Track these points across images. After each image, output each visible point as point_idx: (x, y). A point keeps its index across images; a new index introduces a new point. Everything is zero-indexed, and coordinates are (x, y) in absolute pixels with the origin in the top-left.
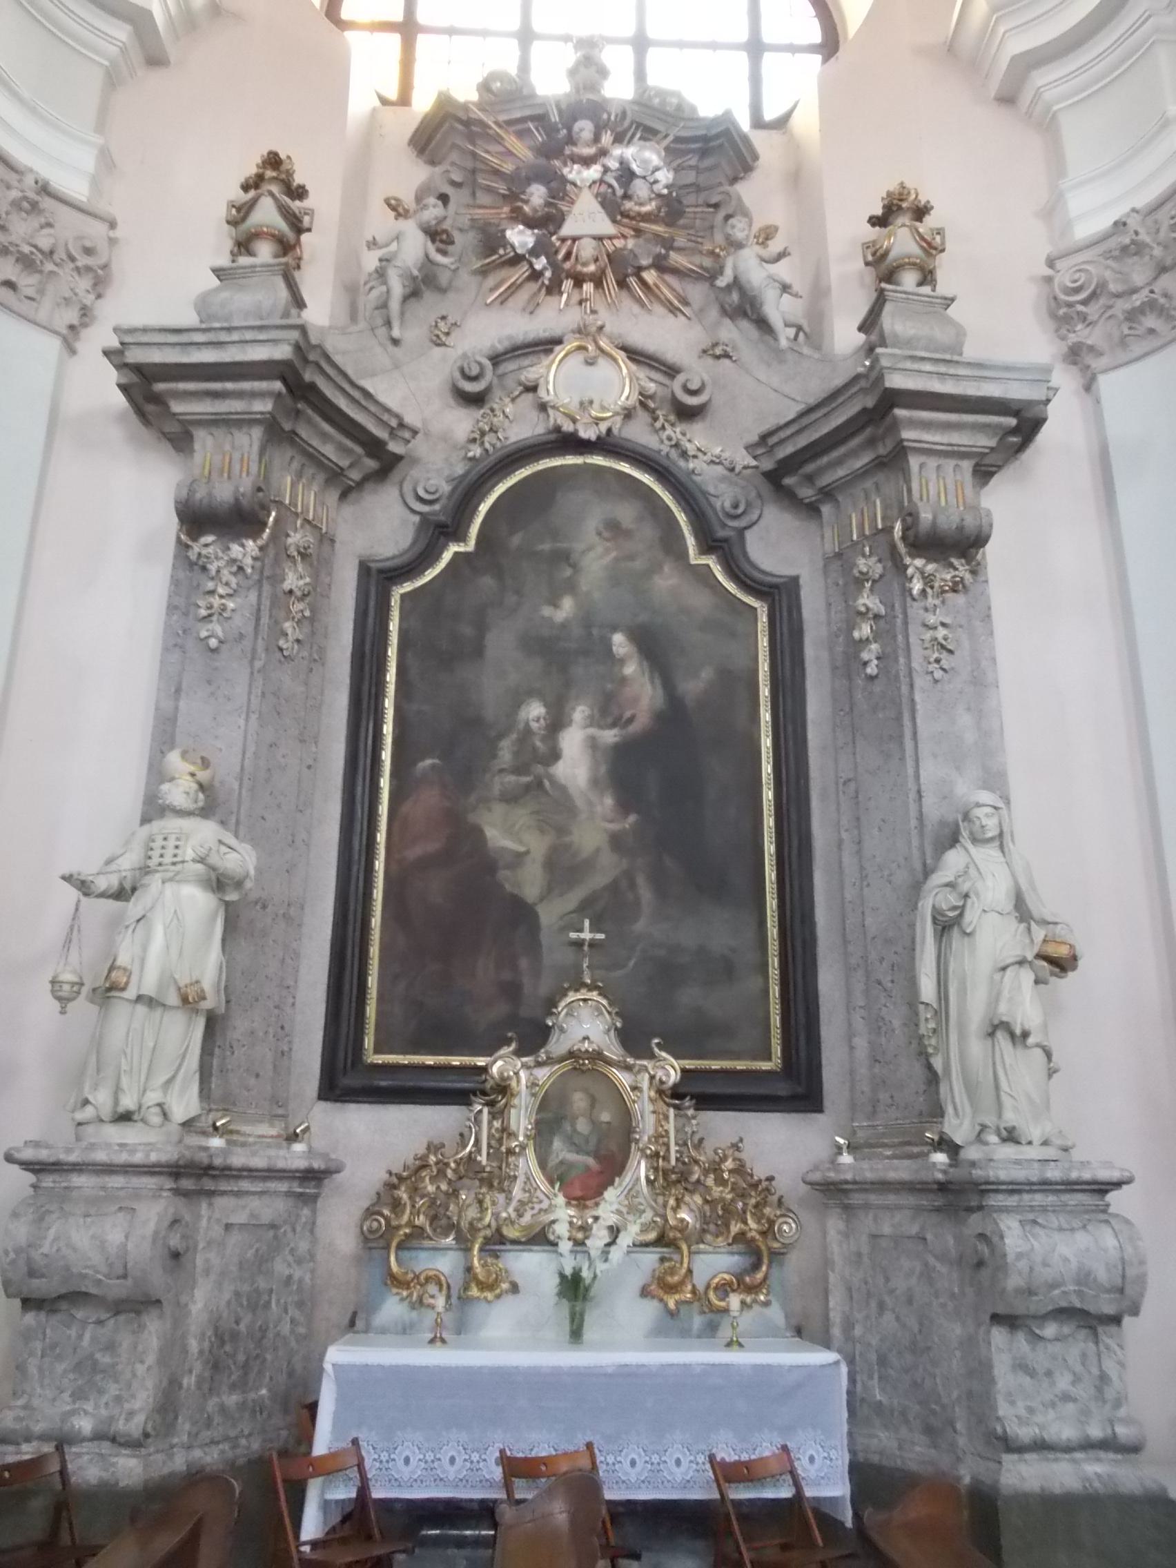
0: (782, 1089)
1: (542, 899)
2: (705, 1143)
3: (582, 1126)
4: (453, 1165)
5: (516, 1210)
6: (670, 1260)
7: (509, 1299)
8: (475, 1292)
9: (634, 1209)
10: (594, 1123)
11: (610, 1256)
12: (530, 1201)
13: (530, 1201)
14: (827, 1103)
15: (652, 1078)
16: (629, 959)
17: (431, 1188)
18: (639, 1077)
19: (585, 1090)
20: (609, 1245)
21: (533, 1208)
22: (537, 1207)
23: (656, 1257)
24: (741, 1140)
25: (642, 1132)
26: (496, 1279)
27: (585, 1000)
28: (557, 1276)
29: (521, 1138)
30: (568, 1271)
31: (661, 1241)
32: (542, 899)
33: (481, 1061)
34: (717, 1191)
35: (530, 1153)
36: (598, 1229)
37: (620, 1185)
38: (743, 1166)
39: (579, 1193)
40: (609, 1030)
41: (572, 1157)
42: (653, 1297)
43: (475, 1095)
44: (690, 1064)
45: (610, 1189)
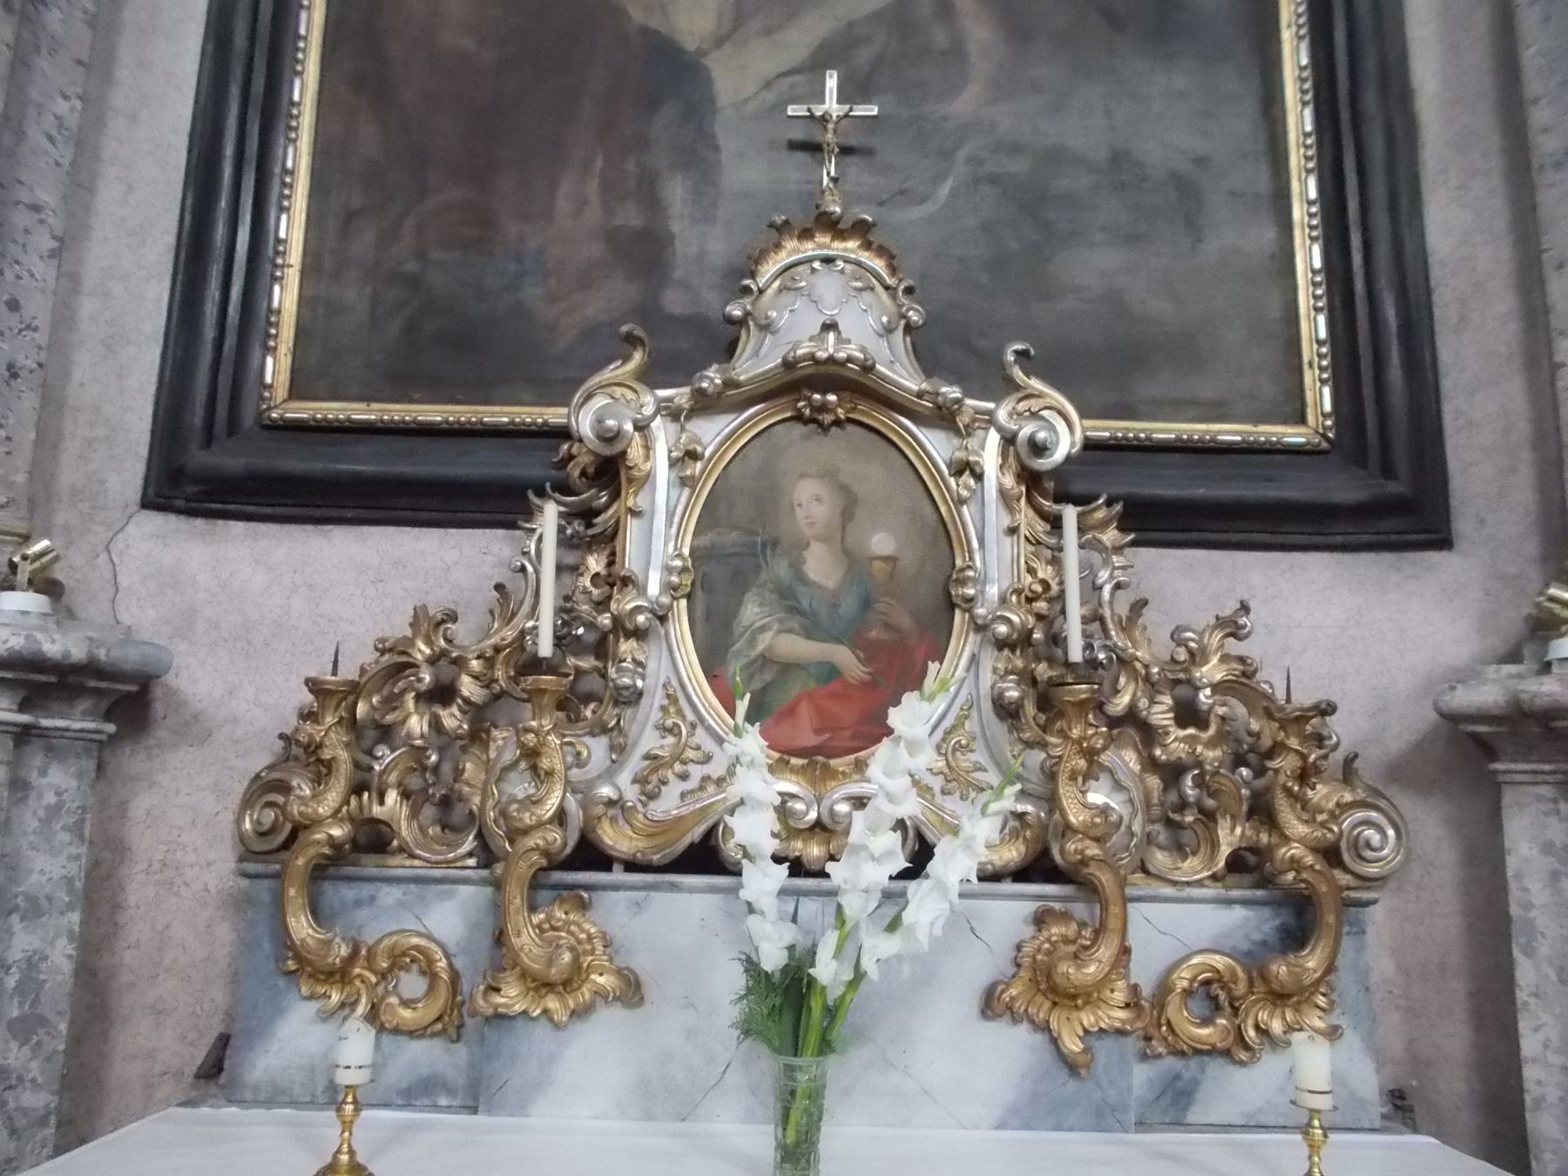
0: (1344, 488)
1: (720, 41)
2: (1149, 615)
3: (821, 567)
4: (475, 665)
5: (640, 780)
6: (1065, 917)
7: (610, 1018)
8: (511, 996)
9: (957, 781)
10: (854, 561)
11: (907, 917)
12: (678, 757)
13: (678, 757)
14: (1462, 524)
15: (1009, 440)
16: (937, 180)
17: (417, 724)
18: (972, 443)
19: (829, 475)
20: (905, 875)
21: (684, 777)
22: (696, 772)
23: (1030, 907)
24: (1245, 608)
25: (981, 581)
26: (576, 962)
27: (828, 260)
28: (739, 968)
29: (654, 589)
30: (772, 959)
31: (1037, 868)
32: (720, 41)
33: (554, 415)
34: (1176, 743)
35: (681, 629)
36: (873, 830)
37: (944, 686)
38: (1249, 674)
39: (811, 740)
40: (889, 330)
41: (796, 646)
42: (1015, 1019)
43: (541, 493)
44: (1104, 429)
45: (910, 698)
